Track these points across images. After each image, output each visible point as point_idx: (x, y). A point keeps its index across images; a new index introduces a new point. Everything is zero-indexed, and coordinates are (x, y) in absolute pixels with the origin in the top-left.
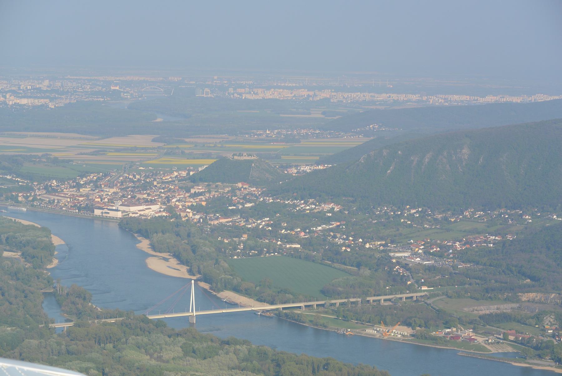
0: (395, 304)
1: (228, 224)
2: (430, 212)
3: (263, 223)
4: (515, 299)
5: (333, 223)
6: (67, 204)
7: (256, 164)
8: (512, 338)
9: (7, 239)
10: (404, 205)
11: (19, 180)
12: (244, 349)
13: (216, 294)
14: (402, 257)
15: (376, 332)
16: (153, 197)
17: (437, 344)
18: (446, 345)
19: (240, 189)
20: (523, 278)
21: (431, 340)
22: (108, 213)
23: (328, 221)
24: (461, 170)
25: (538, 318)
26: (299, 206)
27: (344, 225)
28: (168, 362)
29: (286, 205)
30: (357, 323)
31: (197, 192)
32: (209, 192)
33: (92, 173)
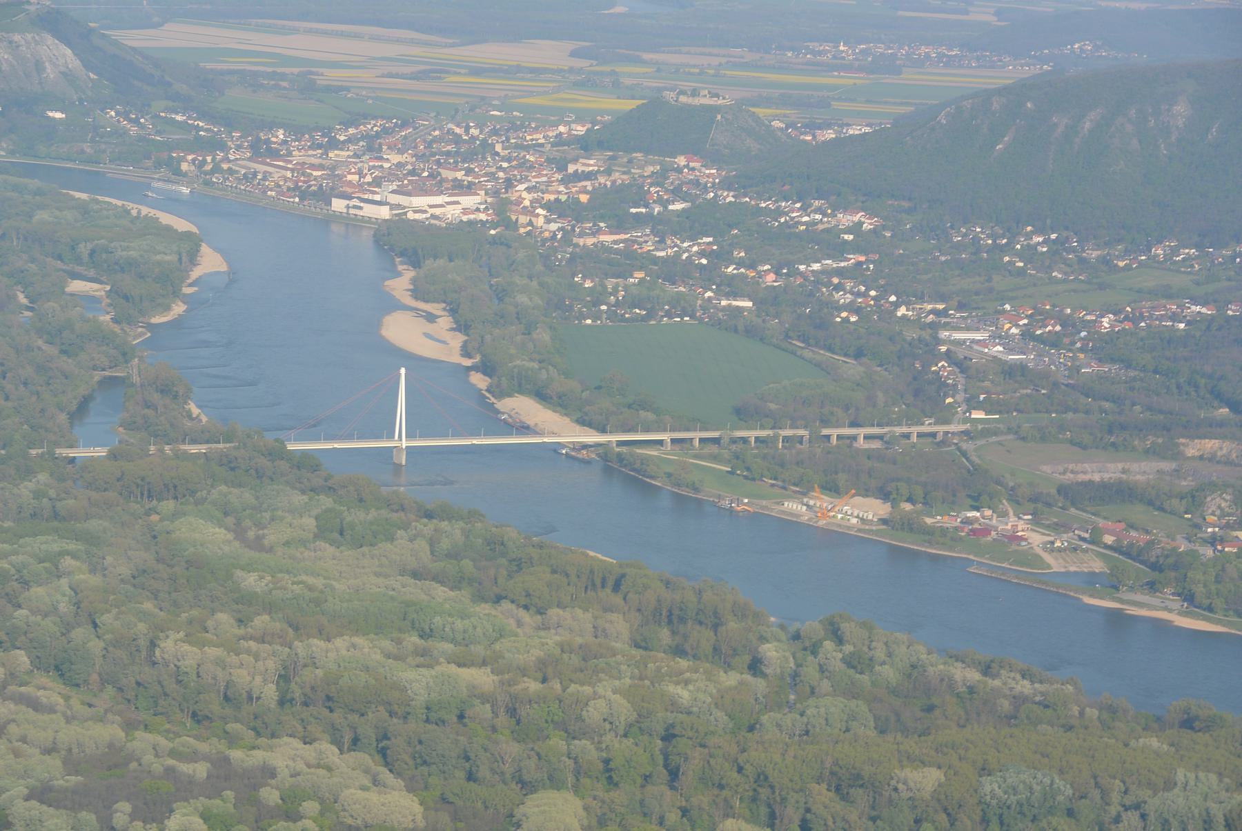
0: (887, 449)
1: (616, 246)
2: (1076, 244)
3: (690, 249)
4: (1170, 452)
5: (852, 256)
6: (281, 183)
7: (725, 115)
8: (1109, 539)
9: (92, 253)
10: (1020, 225)
11: (201, 124)
12: (453, 532)
13: (495, 401)
14: (964, 341)
15: (804, 508)
16: (477, 176)
17: (930, 543)
18: (951, 549)
19: (679, 170)
20: (1216, 404)
21: (923, 533)
22: (361, 208)
23: (839, 250)
24: (1165, 152)
25: (1193, 497)
26: (787, 214)
27: (872, 262)
28: (270, 550)
29: (759, 211)
30: (773, 485)
31: (580, 171)
32: (608, 172)
33: (375, 118)
